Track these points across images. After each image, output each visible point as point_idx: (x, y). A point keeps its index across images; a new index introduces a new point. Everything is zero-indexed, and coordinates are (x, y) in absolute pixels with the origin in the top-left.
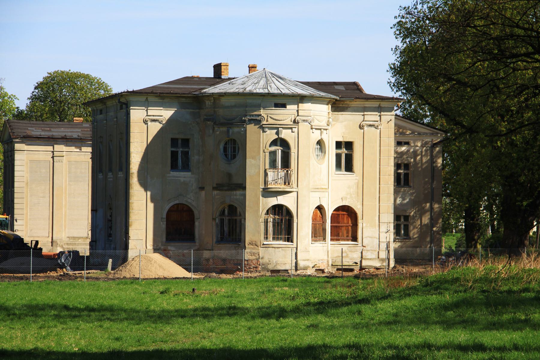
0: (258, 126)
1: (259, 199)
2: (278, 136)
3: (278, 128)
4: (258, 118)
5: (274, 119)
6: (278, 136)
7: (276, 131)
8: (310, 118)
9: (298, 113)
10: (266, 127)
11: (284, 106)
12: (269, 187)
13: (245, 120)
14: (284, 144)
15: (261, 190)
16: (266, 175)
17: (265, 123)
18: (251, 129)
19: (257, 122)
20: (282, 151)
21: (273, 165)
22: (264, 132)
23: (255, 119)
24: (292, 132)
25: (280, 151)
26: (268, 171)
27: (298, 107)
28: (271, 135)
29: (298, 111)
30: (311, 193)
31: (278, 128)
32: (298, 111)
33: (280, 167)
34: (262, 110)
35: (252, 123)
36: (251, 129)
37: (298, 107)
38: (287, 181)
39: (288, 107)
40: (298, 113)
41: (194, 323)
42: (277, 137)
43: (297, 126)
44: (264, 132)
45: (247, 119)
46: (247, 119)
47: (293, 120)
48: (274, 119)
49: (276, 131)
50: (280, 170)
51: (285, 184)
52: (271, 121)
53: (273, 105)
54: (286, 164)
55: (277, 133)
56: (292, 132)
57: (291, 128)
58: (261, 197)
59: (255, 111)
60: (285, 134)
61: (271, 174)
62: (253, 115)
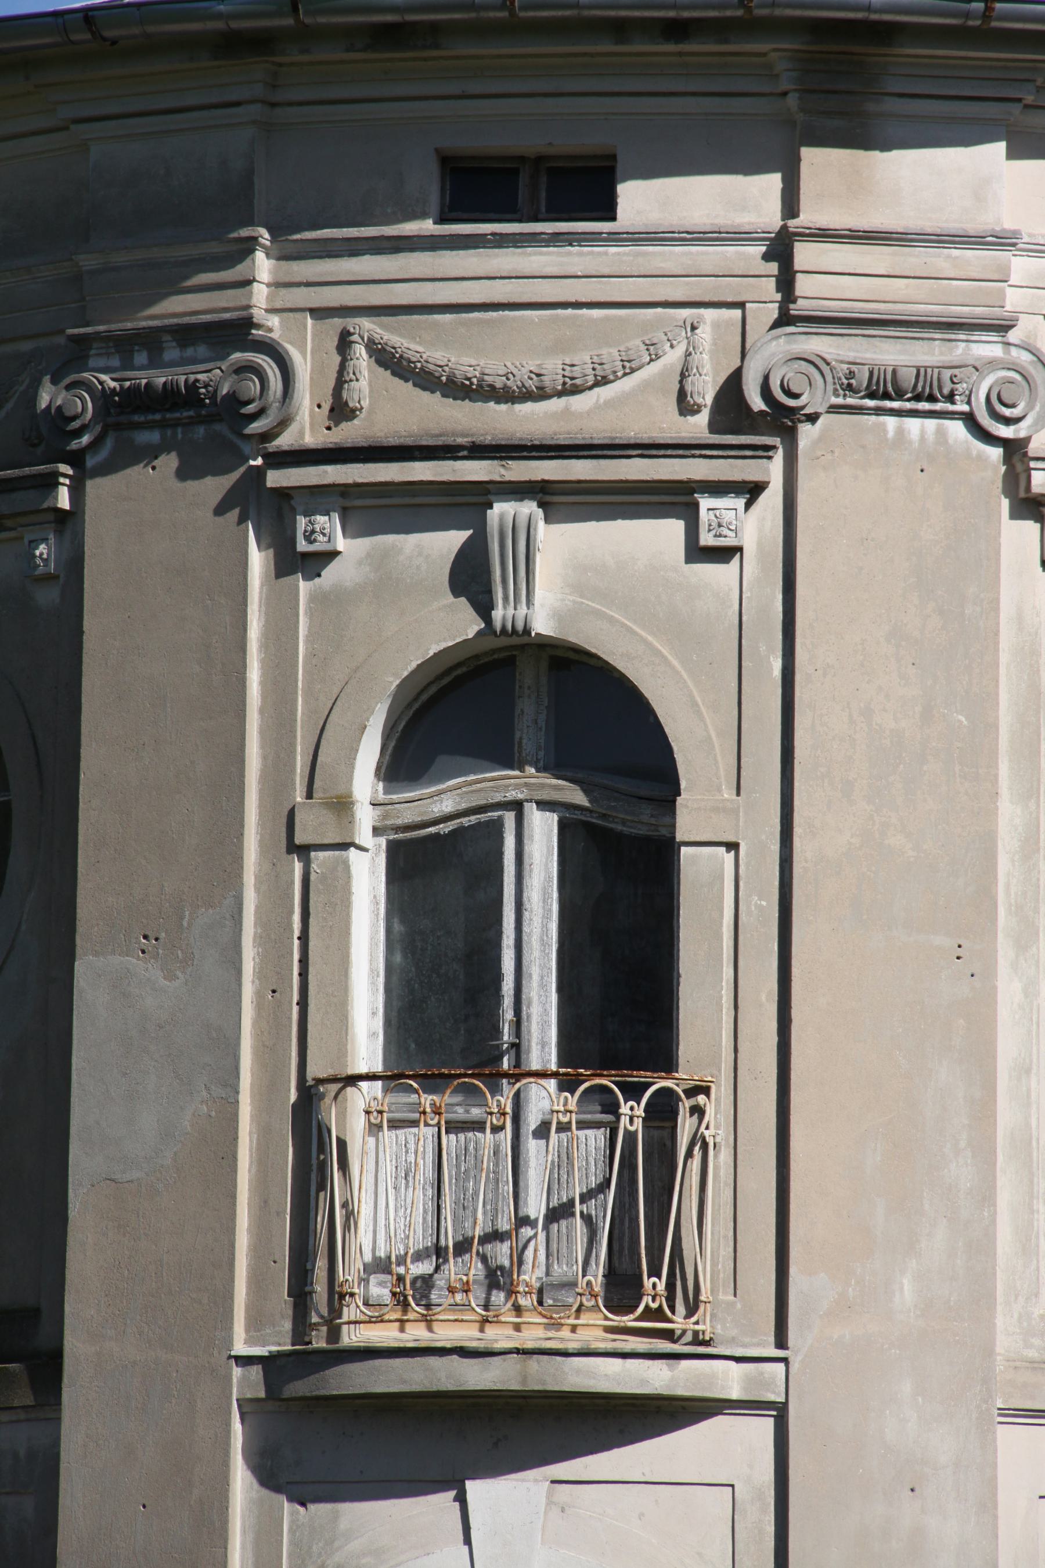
0: (214, 487)
1: (231, 1369)
2: (484, 608)
3: (467, 503)
4: (214, 376)
5: (426, 379)
6: (484, 608)
7: (455, 539)
8: (986, 348)
9: (786, 283)
10: (320, 498)
11: (582, 191)
12: (352, 1337)
13: (60, 421)
14: (588, 721)
15: (246, 1384)
16: (314, 1158)
17: (307, 428)
18: (138, 520)
19: (206, 424)
20: (573, 831)
21: (447, 1029)
22: (296, 562)
23: (170, 392)
24: (698, 552)
25: (543, 831)
26: (352, 1115)
27: (791, 205)
28: (391, 602)
29: (780, 249)
30: (1014, 1441)
31: (484, 494)
32: (780, 249)
33: (543, 1047)
34: (263, 266)
35: (149, 454)
36: (138, 520)
37: (791, 205)
38: (638, 1262)
39: (638, 200)
40: (786, 283)
41: (506, 375)
42: (470, 626)
43: (936, 371)
44: (296, 562)
45: (84, 406)
46: (84, 406)
47: (706, 389)
48: (426, 379)
49: (455, 539)
50: (543, 1099)
51: (621, 1290)
52: (387, 408)
53: (427, 181)
54: (625, 1006)
55: (471, 578)
56: (698, 552)
57: (677, 500)
58: (241, 1479)
59: (172, 283)
60: (573, 579)
61: (389, 1192)
62: (151, 341)
